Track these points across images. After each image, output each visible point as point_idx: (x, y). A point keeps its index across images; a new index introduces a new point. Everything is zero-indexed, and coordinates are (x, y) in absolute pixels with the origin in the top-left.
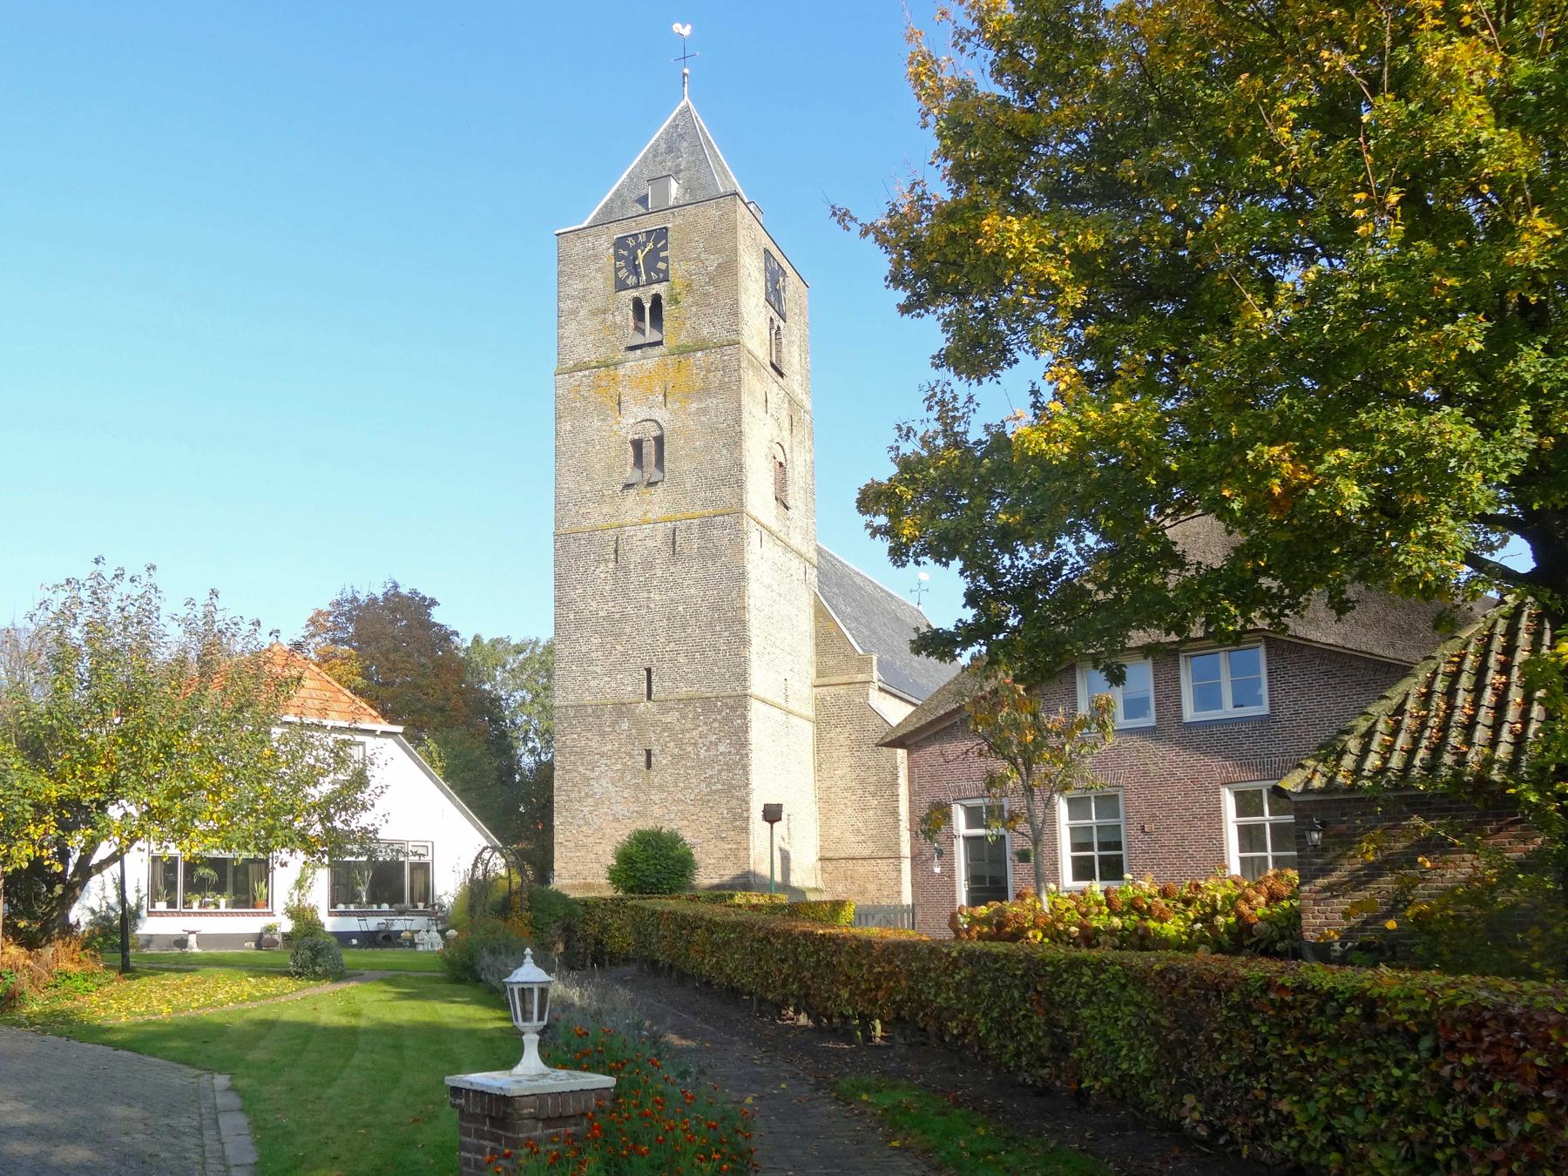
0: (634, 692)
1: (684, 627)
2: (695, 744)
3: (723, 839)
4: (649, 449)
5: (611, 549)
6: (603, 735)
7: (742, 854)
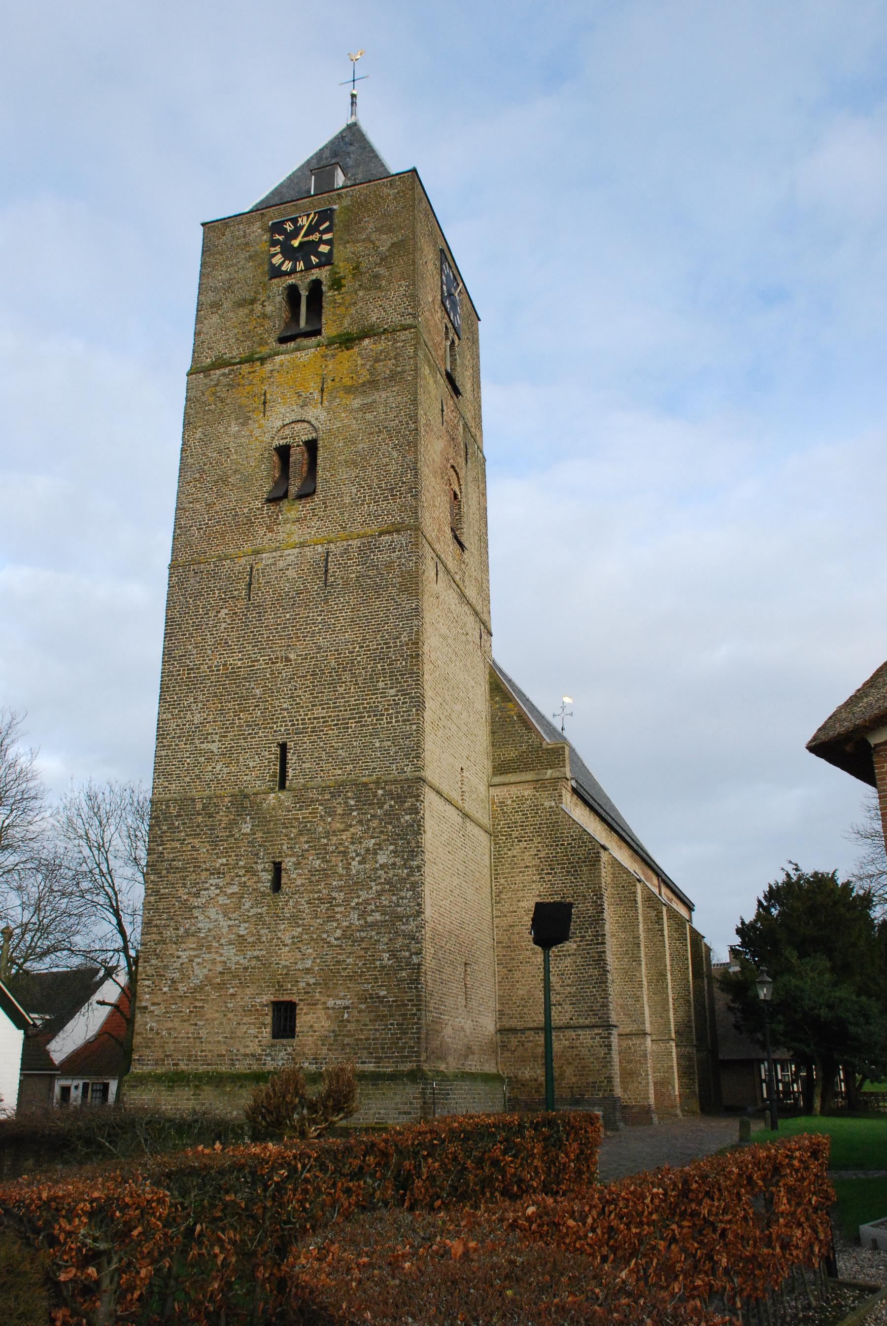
4: (297, 456)
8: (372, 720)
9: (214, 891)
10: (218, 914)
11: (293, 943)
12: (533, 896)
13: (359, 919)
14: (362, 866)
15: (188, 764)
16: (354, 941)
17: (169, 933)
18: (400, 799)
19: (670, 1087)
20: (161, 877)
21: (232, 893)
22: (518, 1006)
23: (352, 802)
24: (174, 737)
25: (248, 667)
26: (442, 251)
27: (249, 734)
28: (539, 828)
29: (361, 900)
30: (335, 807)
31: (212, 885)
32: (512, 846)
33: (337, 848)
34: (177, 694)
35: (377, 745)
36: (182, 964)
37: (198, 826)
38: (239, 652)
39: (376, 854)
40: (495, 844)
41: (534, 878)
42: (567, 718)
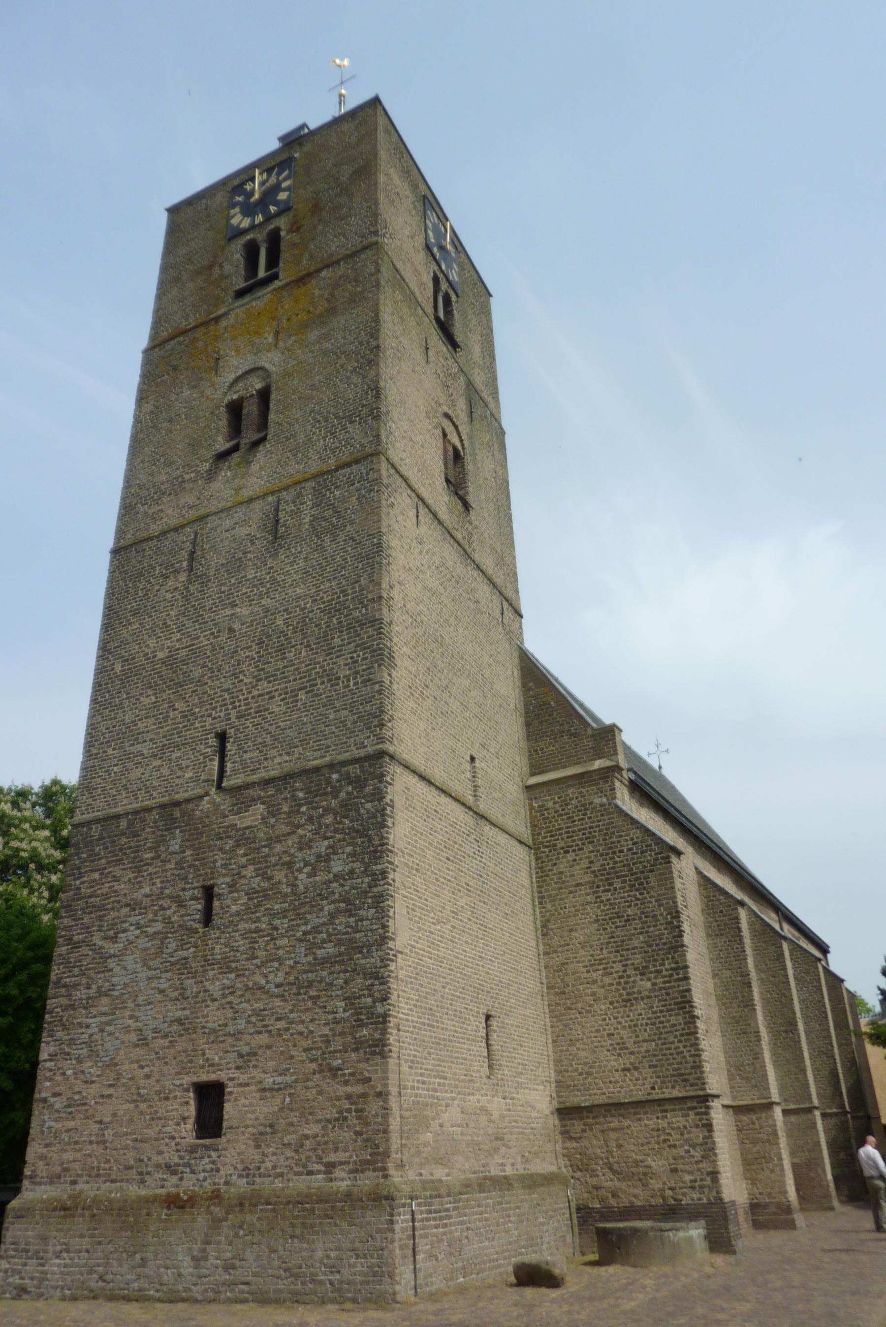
0: (196, 779)
1: (281, 651)
2: (289, 865)
3: (334, 1072)
4: (251, 409)
5: (185, 554)
6: (138, 867)
7: (374, 1106)
8: (326, 687)
9: (134, 932)
10: (136, 962)
11: (224, 996)
12: (590, 922)
13: (306, 956)
14: (312, 880)
15: (115, 773)
16: (299, 988)
17: (80, 994)
18: (359, 783)
19: (820, 1171)
20: (75, 920)
21: (155, 933)
22: (581, 1074)
23: (301, 795)
24: (102, 743)
25: (187, 647)
26: (425, 197)
27: (184, 727)
28: (590, 833)
29: (309, 927)
30: (279, 804)
31: (131, 925)
32: (558, 859)
33: (280, 858)
34: (109, 692)
35: (332, 717)
36: (91, 1036)
37: (121, 850)
38: (178, 632)
39: (328, 860)
40: (537, 859)
41: (589, 898)
42: (664, 757)
